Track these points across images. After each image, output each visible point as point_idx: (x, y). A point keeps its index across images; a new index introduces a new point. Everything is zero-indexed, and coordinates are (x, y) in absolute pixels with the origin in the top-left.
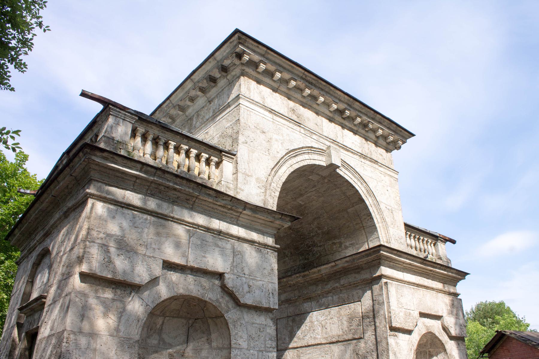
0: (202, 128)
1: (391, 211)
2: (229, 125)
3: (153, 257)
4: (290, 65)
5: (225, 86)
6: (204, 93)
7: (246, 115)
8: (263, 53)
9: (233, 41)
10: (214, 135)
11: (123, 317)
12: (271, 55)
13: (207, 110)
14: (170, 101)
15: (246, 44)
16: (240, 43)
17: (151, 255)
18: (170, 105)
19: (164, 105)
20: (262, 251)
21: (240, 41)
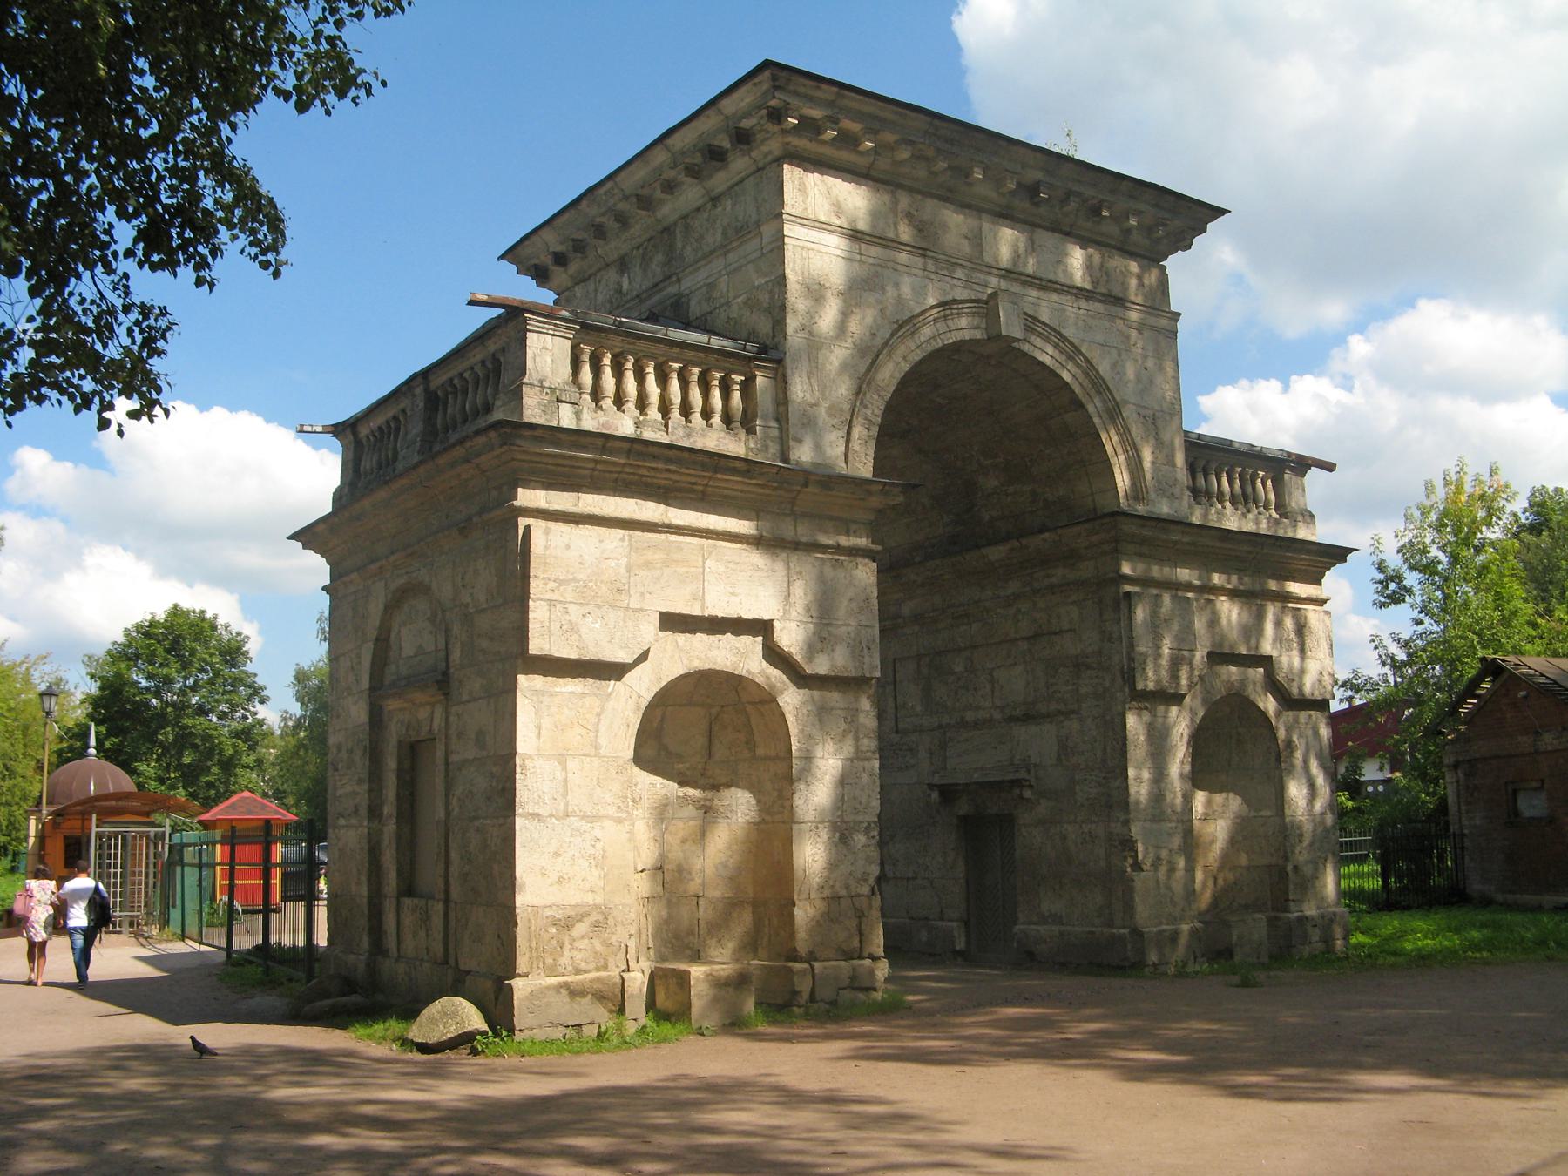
0: (699, 268)
1: (1150, 420)
2: (763, 281)
3: (641, 609)
4: (896, 113)
5: (748, 172)
6: (697, 178)
7: (798, 261)
8: (831, 97)
9: (760, 82)
10: (731, 295)
11: (602, 722)
12: (852, 102)
13: (708, 220)
14: (616, 183)
15: (791, 88)
16: (776, 88)
17: (639, 607)
18: (616, 191)
19: (601, 191)
20: (845, 564)
21: (777, 84)
